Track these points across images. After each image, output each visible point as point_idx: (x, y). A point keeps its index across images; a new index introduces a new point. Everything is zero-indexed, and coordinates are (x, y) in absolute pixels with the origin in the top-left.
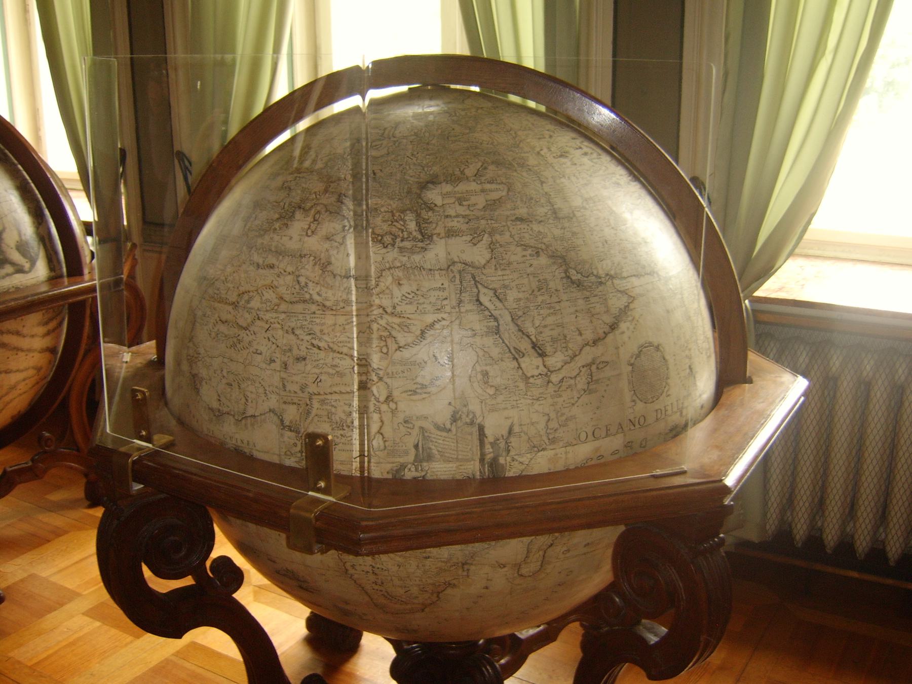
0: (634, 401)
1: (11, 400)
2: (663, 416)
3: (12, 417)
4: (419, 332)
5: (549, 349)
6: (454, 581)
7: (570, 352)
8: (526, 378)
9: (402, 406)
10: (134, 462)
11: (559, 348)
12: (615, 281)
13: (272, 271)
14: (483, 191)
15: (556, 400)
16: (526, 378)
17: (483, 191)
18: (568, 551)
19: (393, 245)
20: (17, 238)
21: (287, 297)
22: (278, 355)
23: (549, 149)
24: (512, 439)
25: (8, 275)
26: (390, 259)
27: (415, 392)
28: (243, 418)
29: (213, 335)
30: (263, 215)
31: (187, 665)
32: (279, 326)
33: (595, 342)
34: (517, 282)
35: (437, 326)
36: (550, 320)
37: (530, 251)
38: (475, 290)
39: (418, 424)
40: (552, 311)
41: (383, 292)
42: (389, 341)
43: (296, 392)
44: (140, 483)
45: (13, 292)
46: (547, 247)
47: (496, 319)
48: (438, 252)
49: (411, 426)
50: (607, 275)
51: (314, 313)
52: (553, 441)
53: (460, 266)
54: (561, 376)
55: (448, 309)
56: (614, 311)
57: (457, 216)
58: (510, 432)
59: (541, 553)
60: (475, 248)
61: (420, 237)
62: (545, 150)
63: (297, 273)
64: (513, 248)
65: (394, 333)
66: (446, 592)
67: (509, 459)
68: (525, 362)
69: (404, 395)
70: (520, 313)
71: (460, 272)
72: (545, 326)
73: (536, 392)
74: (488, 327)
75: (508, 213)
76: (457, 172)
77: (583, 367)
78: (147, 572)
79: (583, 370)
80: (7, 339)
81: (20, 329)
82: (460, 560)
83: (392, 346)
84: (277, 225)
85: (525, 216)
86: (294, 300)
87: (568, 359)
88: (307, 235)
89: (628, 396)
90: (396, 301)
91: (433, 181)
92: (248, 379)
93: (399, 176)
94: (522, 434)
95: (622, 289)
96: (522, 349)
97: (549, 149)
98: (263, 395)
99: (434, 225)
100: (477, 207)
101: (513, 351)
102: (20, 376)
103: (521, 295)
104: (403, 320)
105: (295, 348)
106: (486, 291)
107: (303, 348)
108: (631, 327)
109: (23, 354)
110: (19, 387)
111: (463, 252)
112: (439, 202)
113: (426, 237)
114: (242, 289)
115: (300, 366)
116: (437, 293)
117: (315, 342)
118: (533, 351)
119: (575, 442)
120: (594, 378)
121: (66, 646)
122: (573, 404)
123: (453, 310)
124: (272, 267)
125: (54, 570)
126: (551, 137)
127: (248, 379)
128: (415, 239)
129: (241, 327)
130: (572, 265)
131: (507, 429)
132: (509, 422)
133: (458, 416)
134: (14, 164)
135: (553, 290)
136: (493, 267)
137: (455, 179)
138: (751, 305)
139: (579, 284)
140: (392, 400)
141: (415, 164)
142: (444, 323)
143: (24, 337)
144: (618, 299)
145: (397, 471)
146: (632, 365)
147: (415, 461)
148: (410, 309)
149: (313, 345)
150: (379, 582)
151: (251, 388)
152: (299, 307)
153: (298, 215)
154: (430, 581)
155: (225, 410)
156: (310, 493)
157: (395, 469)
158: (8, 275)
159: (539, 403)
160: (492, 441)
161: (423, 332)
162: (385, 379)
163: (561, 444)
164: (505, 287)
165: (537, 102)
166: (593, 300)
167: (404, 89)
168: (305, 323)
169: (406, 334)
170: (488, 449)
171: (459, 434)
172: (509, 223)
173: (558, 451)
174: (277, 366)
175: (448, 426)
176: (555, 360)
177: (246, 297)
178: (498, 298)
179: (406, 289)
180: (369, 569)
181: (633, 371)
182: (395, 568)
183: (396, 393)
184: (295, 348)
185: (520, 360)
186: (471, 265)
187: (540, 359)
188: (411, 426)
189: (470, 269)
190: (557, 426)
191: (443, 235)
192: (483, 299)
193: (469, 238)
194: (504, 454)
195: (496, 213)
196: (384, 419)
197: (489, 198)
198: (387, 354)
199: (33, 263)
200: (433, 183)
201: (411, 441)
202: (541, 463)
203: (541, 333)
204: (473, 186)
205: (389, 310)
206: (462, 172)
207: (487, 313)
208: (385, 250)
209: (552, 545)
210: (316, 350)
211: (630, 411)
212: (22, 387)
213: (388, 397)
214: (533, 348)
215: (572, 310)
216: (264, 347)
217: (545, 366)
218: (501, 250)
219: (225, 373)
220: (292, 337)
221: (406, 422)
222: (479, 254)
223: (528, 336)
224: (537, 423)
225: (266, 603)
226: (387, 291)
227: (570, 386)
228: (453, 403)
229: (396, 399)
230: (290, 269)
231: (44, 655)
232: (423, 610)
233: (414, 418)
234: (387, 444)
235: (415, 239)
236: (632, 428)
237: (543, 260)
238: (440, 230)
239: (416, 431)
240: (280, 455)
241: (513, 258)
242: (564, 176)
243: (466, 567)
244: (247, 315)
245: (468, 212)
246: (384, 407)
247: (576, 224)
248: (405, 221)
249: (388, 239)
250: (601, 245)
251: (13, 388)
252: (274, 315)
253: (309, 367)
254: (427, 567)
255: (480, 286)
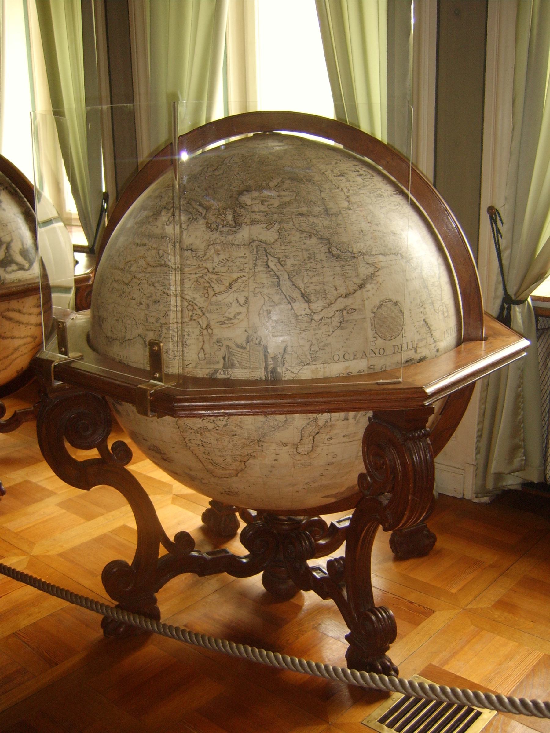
0: (375, 337)
1: (16, 359)
2: (400, 351)
3: (18, 372)
4: (228, 285)
5: (313, 298)
6: (254, 454)
7: (328, 301)
8: (296, 316)
9: (216, 331)
10: (55, 366)
11: (320, 298)
12: (365, 256)
13: (144, 248)
14: (279, 196)
15: (317, 332)
16: (296, 316)
17: (279, 196)
18: (331, 438)
19: (217, 230)
20: (20, 247)
21: (152, 264)
22: (144, 300)
23: (332, 171)
24: (286, 356)
25: (13, 271)
26: (214, 238)
27: (224, 323)
28: (125, 341)
29: (110, 289)
30: (145, 213)
31: (118, 538)
32: (146, 282)
33: (346, 296)
34: (294, 254)
35: (240, 280)
36: (315, 279)
37: (305, 235)
38: (266, 258)
39: (226, 343)
40: (316, 273)
41: (208, 259)
42: (209, 289)
43: (153, 323)
44: (60, 380)
45: (17, 283)
46: (318, 232)
47: (278, 277)
48: (244, 234)
49: (221, 344)
50: (360, 252)
51: (166, 273)
52: (315, 359)
53: (257, 243)
54: (321, 316)
55: (247, 270)
56: (362, 276)
57: (259, 212)
58: (285, 350)
59: (311, 438)
60: (268, 232)
61: (234, 224)
62: (329, 171)
63: (158, 248)
64: (293, 232)
65: (213, 285)
66: (248, 462)
67: (284, 369)
68: (296, 305)
69: (217, 324)
70: (294, 274)
71: (257, 247)
72: (311, 283)
73: (303, 326)
74: (272, 282)
75: (294, 210)
76: (264, 184)
77: (337, 311)
78: (67, 445)
79: (337, 313)
80: (12, 314)
81: (21, 308)
82: (256, 438)
83: (211, 293)
84: (151, 219)
85: (305, 212)
86: (155, 265)
87: (326, 305)
88: (167, 225)
89: (370, 333)
90: (215, 264)
91: (248, 190)
92: (127, 316)
93: (226, 187)
94: (293, 353)
95: (370, 262)
96: (295, 297)
97: (332, 171)
98: (135, 326)
99: (244, 217)
100: (273, 206)
101: (288, 298)
102: (21, 342)
103: (296, 262)
104: (219, 276)
105: (154, 294)
106: (273, 259)
107: (158, 295)
108: (375, 288)
109: (24, 326)
110: (21, 350)
111: (260, 234)
112: (249, 202)
113: (237, 225)
114: (127, 260)
115: (156, 306)
116: (242, 260)
117: (166, 291)
118: (302, 298)
119: (330, 361)
120: (345, 319)
121: (40, 523)
122: (329, 335)
123: (250, 271)
124: (144, 245)
125: (42, 478)
126: (336, 163)
127: (127, 316)
128: (230, 226)
129: (125, 283)
130: (334, 244)
131: (283, 348)
132: (283, 345)
133: (250, 339)
134: (21, 197)
135: (318, 260)
136: (279, 244)
137: (260, 189)
138: (532, 303)
139: (337, 257)
140: (210, 328)
141: (238, 179)
142: (244, 278)
143: (24, 314)
144: (367, 268)
145: (212, 374)
146: (374, 313)
147: (224, 367)
148: (223, 270)
149: (164, 293)
150: (207, 453)
151: (129, 322)
152: (158, 269)
153: (163, 213)
154: (238, 453)
155: (115, 337)
156: (152, 381)
157: (211, 372)
158: (13, 271)
159: (305, 333)
160: (273, 356)
161: (230, 284)
162: (206, 314)
163: (320, 361)
164: (286, 257)
165: (336, 141)
166: (347, 268)
167: (251, 134)
168: (160, 279)
169: (220, 286)
170: (270, 361)
171: (251, 351)
172: (293, 216)
173: (318, 366)
174: (143, 306)
175: (244, 345)
176: (317, 305)
177: (129, 264)
178: (280, 264)
179: (222, 257)
180: (200, 443)
181: (375, 317)
182: (216, 442)
183: (212, 323)
184: (154, 294)
185: (292, 304)
186: (265, 242)
187: (306, 304)
188: (221, 344)
189: (264, 244)
190: (317, 349)
191: (248, 223)
192: (270, 264)
193: (265, 225)
194: (281, 365)
195: (285, 210)
196: (205, 339)
197: (282, 200)
198: (207, 298)
199: (31, 264)
200: (247, 191)
201: (220, 354)
202: (306, 373)
203: (308, 287)
204: (273, 194)
205: (211, 270)
206: (267, 184)
207: (272, 273)
208: (211, 233)
209: (318, 432)
210: (165, 296)
211: (372, 344)
212: (23, 350)
213: (207, 326)
214: (302, 296)
215: (332, 273)
216: (136, 295)
217: (310, 309)
218: (286, 233)
219: (115, 313)
220: (152, 288)
221: (218, 342)
222: (270, 236)
223: (299, 289)
224: (304, 346)
225: (180, 506)
226: (211, 258)
227: (327, 323)
228: (248, 330)
229: (212, 327)
230: (154, 246)
231: (26, 527)
232: (237, 475)
233: (223, 339)
234: (206, 355)
235: (230, 226)
236: (374, 355)
237: (314, 240)
238: (247, 220)
239: (223, 349)
240: (144, 364)
241: (293, 239)
242: (338, 188)
243: (260, 443)
244: (129, 276)
245: (266, 209)
246: (205, 332)
247: (341, 219)
248: (225, 215)
249: (214, 226)
250: (357, 233)
251: (16, 349)
252: (144, 275)
253: (161, 306)
254: (235, 442)
255: (269, 256)
